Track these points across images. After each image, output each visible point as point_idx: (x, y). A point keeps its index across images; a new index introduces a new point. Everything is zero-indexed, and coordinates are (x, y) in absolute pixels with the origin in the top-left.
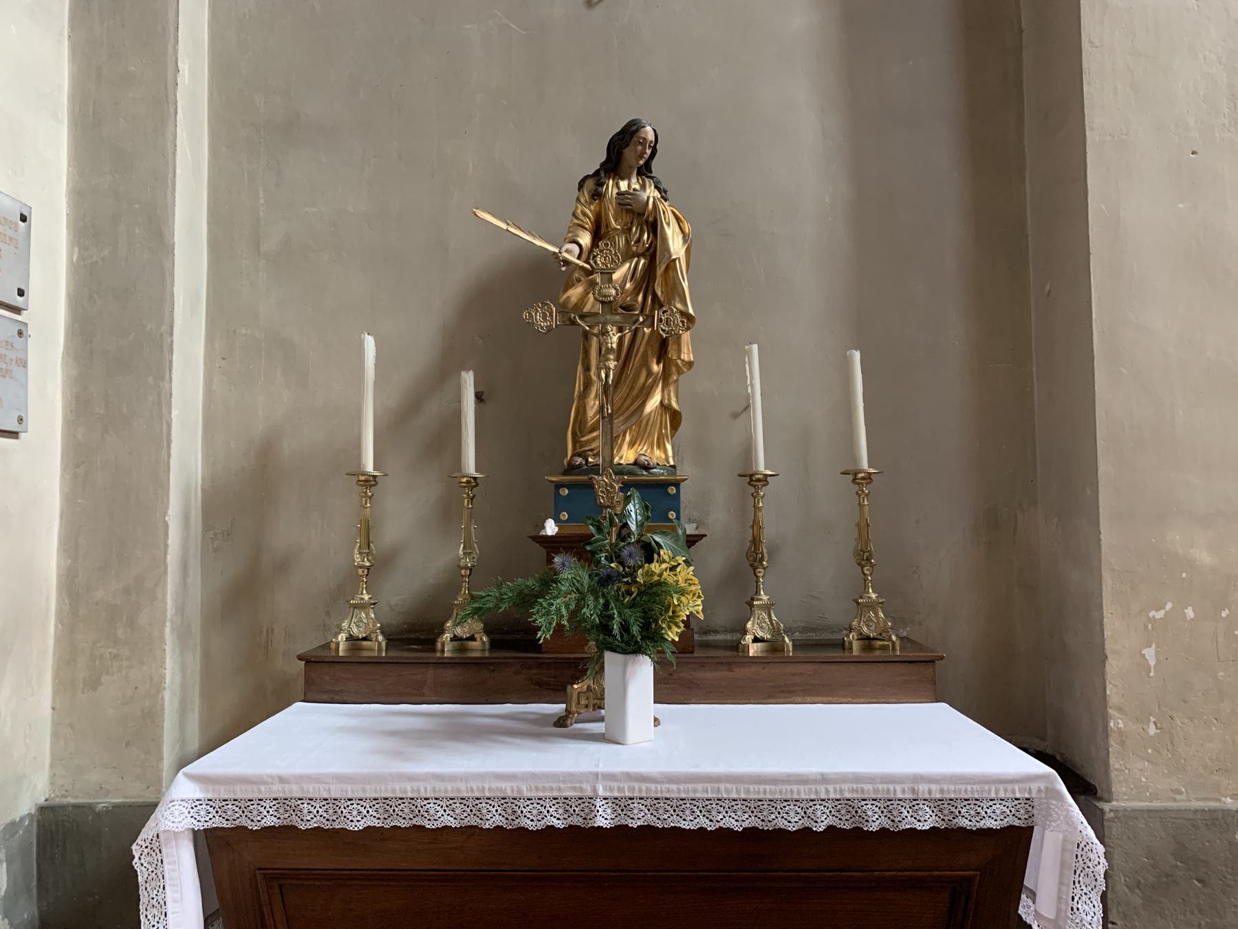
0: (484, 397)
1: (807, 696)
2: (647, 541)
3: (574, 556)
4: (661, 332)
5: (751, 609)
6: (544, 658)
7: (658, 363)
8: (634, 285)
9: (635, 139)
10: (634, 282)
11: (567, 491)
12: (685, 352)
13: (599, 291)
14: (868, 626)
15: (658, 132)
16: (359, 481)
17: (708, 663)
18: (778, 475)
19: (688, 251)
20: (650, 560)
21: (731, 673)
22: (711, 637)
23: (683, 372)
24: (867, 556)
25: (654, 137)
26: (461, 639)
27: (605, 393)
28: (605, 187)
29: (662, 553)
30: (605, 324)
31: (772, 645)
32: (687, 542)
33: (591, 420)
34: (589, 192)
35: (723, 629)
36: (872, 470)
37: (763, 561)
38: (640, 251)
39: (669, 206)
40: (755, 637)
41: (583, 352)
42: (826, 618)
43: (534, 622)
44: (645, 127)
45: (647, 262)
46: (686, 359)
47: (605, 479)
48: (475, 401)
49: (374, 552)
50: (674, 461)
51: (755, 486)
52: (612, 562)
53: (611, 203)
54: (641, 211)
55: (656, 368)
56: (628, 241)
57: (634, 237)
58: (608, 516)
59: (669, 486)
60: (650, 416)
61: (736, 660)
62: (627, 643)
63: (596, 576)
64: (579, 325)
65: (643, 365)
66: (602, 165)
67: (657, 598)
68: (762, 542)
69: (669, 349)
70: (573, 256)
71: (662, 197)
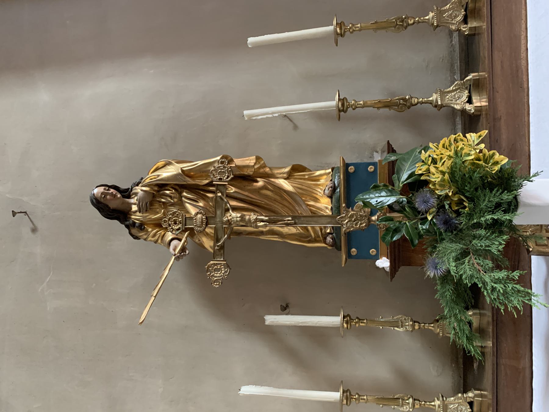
1: (521, 56)
4: (229, 179)
5: (444, 106)
7: (257, 182)
8: (201, 200)
9: (102, 200)
11: (353, 250)
12: (249, 162)
14: (456, 17)
15: (98, 185)
16: (347, 404)
21: (502, 118)
23: (264, 163)
24: (400, 22)
27: (274, 222)
30: (223, 223)
33: (299, 230)
34: (140, 232)
36: (335, 23)
40: (467, 102)
42: (443, 56)
44: (94, 194)
45: (185, 191)
46: (254, 161)
47: (345, 222)
49: (402, 395)
50: (328, 169)
51: (347, 108)
52: (426, 218)
55: (261, 183)
56: (173, 205)
58: (384, 223)
64: (224, 243)
65: (259, 192)
66: (122, 222)
67: (467, 176)
69: (246, 174)
70: (179, 244)
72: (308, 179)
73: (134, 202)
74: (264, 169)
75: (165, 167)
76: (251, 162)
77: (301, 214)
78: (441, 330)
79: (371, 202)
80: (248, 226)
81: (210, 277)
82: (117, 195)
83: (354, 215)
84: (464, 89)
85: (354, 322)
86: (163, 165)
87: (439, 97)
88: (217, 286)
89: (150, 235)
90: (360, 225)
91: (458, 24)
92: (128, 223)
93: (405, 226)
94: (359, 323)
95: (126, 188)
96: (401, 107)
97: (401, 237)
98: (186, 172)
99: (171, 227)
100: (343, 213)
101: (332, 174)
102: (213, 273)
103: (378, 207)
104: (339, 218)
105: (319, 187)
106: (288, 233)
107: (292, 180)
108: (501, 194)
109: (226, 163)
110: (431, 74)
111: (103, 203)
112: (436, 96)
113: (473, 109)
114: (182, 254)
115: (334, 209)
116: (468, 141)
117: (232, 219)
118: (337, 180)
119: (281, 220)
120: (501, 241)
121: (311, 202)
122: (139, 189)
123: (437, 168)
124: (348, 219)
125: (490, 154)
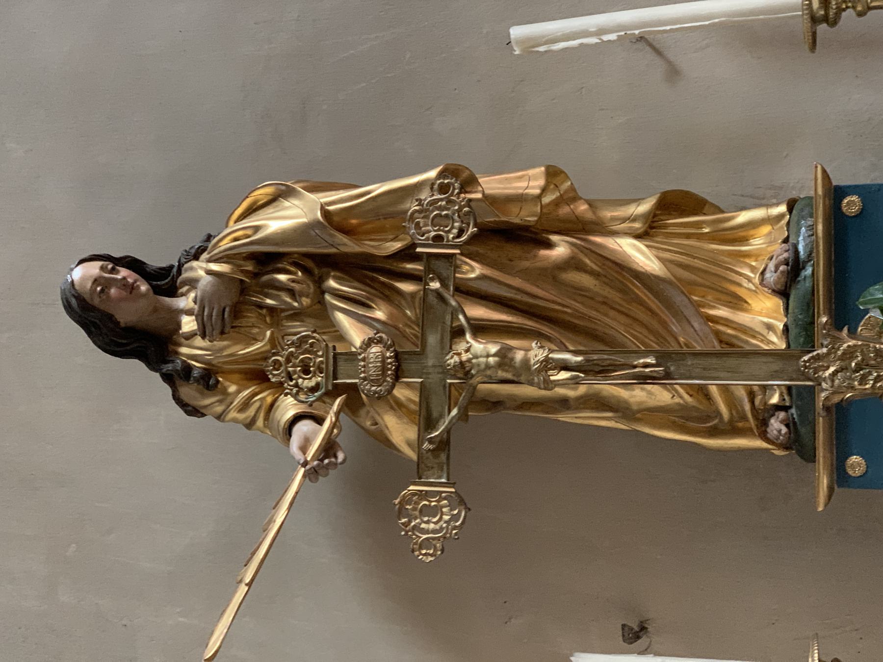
4: (464, 238)
7: (549, 245)
9: (96, 302)
11: (855, 459)
12: (525, 184)
13: (373, 382)
19: (314, 188)
23: (572, 188)
27: (600, 372)
30: (446, 372)
33: (681, 397)
34: (204, 396)
41: (529, 409)
44: (72, 281)
46: (542, 182)
47: (827, 373)
50: (778, 204)
56: (297, 315)
59: (840, 208)
60: (671, 262)
64: (448, 431)
65: (554, 278)
66: (152, 365)
69: (517, 221)
70: (316, 433)
72: (713, 238)
73: (187, 308)
75: (275, 204)
76: (531, 184)
81: (407, 532)
82: (138, 287)
83: (856, 351)
86: (270, 197)
89: (232, 403)
95: (164, 264)
98: (336, 219)
99: (294, 381)
100: (822, 346)
102: (418, 521)
104: (809, 360)
105: (747, 261)
109: (456, 191)
111: (99, 310)
114: (326, 461)
117: (474, 361)
118: (804, 239)
119: (623, 365)
121: (719, 309)
122: (201, 268)
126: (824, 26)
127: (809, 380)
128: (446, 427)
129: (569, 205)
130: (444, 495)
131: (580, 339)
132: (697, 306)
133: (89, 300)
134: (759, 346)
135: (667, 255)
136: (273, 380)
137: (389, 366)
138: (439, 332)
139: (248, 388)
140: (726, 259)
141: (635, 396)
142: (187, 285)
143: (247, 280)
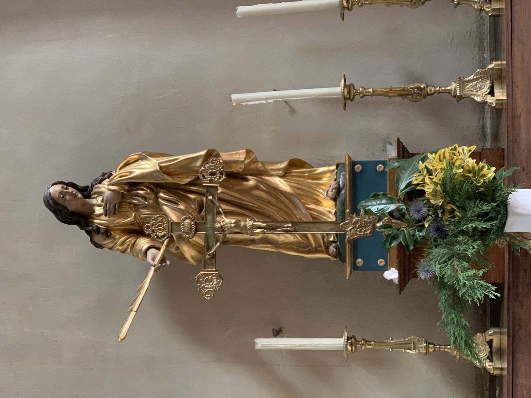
0: (277, 328)
2: (405, 193)
3: (420, 261)
4: (221, 180)
5: (464, 98)
6: (509, 283)
7: (247, 180)
8: (182, 202)
9: (60, 201)
10: (179, 202)
11: (359, 260)
13: (187, 234)
17: (513, 136)
18: (344, 75)
20: (423, 193)
21: (522, 116)
22: (489, 131)
23: (256, 158)
25: (58, 185)
26: (491, 352)
27: (272, 229)
28: (100, 226)
29: (416, 182)
31: (496, 79)
32: (403, 158)
33: (297, 238)
34: (105, 240)
35: (481, 121)
37: (420, 87)
38: (152, 196)
39: (116, 172)
40: (489, 93)
41: (238, 244)
42: (471, 30)
43: (480, 301)
44: (50, 193)
45: (162, 191)
46: (244, 156)
47: (349, 229)
48: (280, 337)
51: (354, 96)
52: (424, 225)
53: (114, 221)
54: (120, 196)
55: (252, 182)
56: (145, 207)
57: (142, 202)
61: (510, 111)
62: (498, 213)
63: (437, 241)
64: (215, 251)
65: (250, 193)
66: (82, 228)
67: (457, 187)
68: (404, 89)
69: (235, 171)
70: (157, 254)
71: (109, 177)
72: (308, 178)
73: (98, 204)
74: (255, 165)
76: (240, 156)
77: (300, 219)
78: (458, 352)
79: (371, 209)
80: (243, 233)
81: (200, 289)
83: (358, 222)
84: (485, 78)
85: (360, 344)
87: (458, 86)
88: (209, 298)
89: (117, 243)
90: (364, 232)
91: (480, 3)
92: (90, 228)
93: (403, 233)
94: (366, 345)
96: (416, 96)
97: (399, 243)
99: (155, 233)
100: (347, 220)
101: (336, 173)
102: (204, 284)
103: (379, 214)
106: (284, 242)
107: (289, 178)
108: (482, 205)
109: (218, 163)
110: (456, 51)
111: (61, 204)
112: (455, 85)
113: (494, 103)
115: (338, 212)
116: (460, 154)
117: (226, 225)
118: (342, 180)
119: (280, 227)
120: (475, 246)
121: (312, 205)
123: (431, 179)
124: (352, 226)
125: (480, 167)
126: (349, 101)
127: (343, 231)
128: (215, 250)
129: (254, 164)
130: (214, 275)
131: (260, 216)
132: (304, 204)
133: (57, 201)
134: (326, 219)
135: (292, 184)
136: (147, 233)
137: (193, 227)
138: (212, 214)
139: (124, 236)
140: (314, 186)
141: (280, 238)
142: (97, 194)
143: (126, 193)
